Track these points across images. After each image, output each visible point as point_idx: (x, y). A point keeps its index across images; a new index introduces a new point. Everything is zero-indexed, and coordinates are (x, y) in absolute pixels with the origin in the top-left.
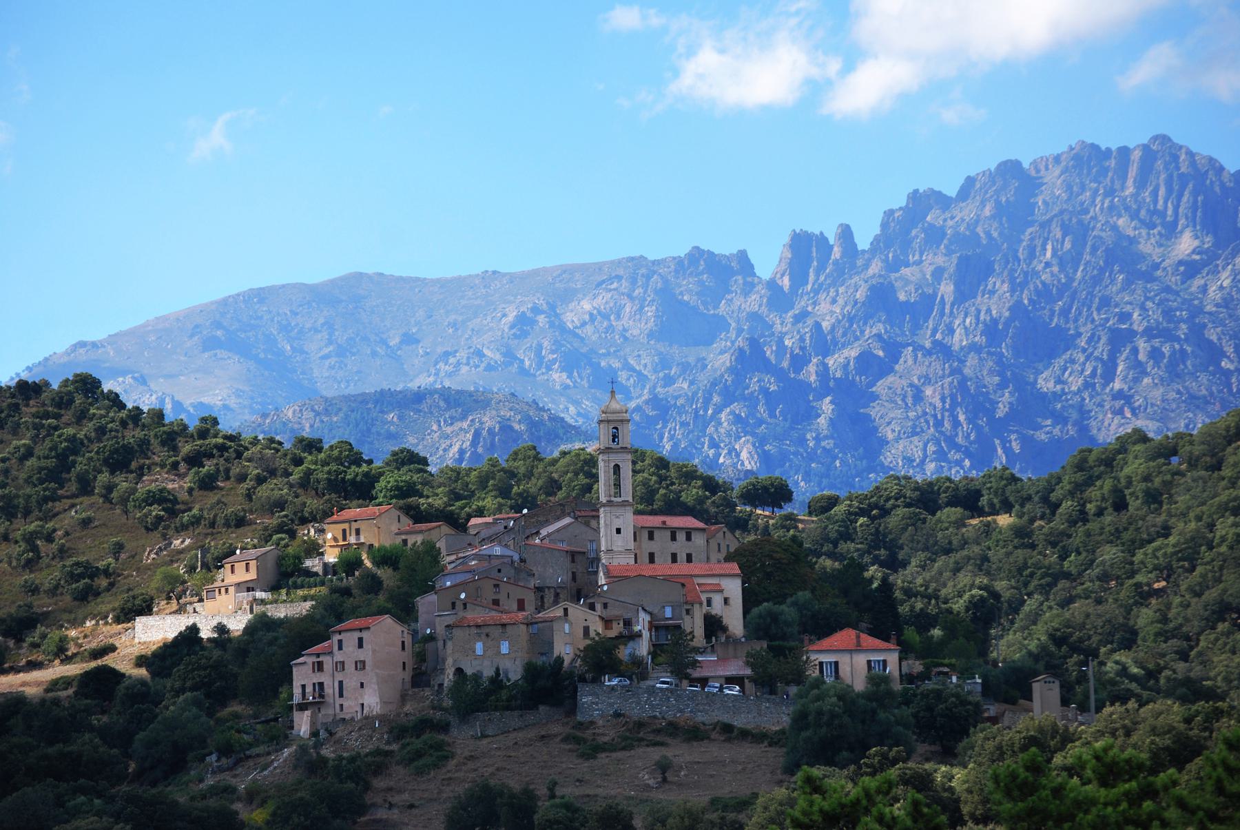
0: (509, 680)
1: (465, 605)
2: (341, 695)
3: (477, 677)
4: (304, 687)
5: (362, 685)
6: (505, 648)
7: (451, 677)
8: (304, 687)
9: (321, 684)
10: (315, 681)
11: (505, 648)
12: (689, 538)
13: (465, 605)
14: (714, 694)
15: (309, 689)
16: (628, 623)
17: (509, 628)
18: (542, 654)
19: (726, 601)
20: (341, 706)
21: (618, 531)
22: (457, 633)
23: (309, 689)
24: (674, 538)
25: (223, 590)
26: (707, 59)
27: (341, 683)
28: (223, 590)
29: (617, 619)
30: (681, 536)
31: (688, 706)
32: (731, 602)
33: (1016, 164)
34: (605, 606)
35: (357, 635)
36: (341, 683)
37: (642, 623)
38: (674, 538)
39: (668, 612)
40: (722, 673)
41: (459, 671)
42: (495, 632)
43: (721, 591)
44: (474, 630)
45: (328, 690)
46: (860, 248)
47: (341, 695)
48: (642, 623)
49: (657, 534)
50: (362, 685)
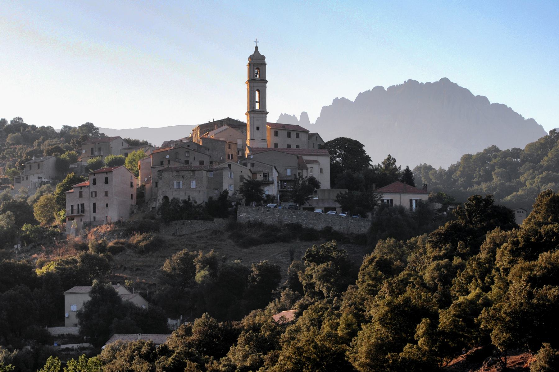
0: (196, 202)
1: (169, 161)
2: (94, 211)
3: (175, 201)
4: (72, 206)
5: (107, 205)
6: (193, 184)
7: (161, 201)
8: (72, 206)
9: (82, 205)
10: (80, 203)
11: (193, 184)
12: (298, 136)
13: (169, 161)
14: (320, 214)
15: (75, 208)
16: (266, 175)
17: (196, 172)
18: (216, 189)
19: (321, 170)
20: (95, 217)
21: (258, 129)
22: (165, 175)
23: (75, 208)
24: (289, 136)
25: (25, 178)
26: (144, 307)
27: (94, 204)
28: (25, 178)
29: (260, 172)
30: (293, 135)
31: (304, 220)
32: (324, 171)
33: (382, 88)
34: (253, 165)
35: (105, 176)
36: (94, 204)
37: (274, 175)
38: (289, 136)
39: (289, 172)
40: (322, 205)
41: (166, 198)
42: (188, 174)
43: (319, 163)
44: (175, 174)
45: (86, 208)
46: (311, 123)
47: (94, 211)
48: (274, 175)
49: (280, 132)
50: (107, 205)
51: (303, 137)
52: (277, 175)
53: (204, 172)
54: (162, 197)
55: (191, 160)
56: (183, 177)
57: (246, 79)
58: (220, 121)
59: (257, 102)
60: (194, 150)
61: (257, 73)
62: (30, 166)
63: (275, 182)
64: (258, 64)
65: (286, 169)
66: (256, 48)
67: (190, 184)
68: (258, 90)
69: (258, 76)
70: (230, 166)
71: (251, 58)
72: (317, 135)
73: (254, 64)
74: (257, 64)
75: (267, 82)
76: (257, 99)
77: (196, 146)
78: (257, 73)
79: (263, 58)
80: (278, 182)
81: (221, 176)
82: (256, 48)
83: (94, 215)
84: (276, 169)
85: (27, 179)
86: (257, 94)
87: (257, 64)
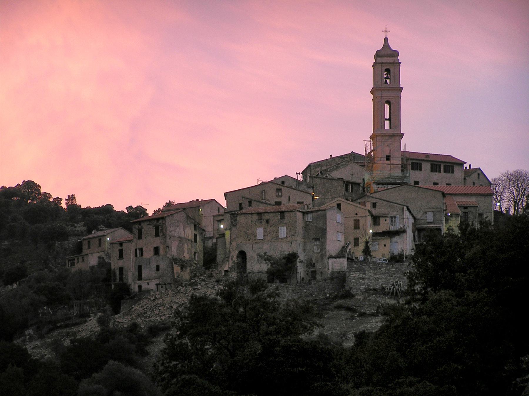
6: (283, 232)
7: (235, 259)
11: (283, 232)
20: (140, 287)
34: (374, 205)
51: (458, 173)
52: (412, 221)
53: (298, 213)
54: (237, 252)
55: (284, 200)
56: (267, 222)
57: (371, 85)
58: (341, 157)
59: (386, 120)
60: (291, 187)
61: (387, 78)
62: (89, 242)
63: (409, 231)
64: (386, 63)
65: (426, 213)
66: (386, 39)
67: (277, 232)
68: (388, 102)
69: (388, 81)
70: (339, 206)
71: (378, 55)
72: (480, 172)
73: (382, 63)
74: (387, 63)
75: (401, 89)
76: (387, 116)
77: (295, 183)
78: (387, 78)
79: (396, 54)
80: (414, 233)
81: (325, 217)
82: (386, 39)
83: (139, 282)
84: (410, 212)
85: (83, 260)
86: (387, 107)
87: (387, 63)
